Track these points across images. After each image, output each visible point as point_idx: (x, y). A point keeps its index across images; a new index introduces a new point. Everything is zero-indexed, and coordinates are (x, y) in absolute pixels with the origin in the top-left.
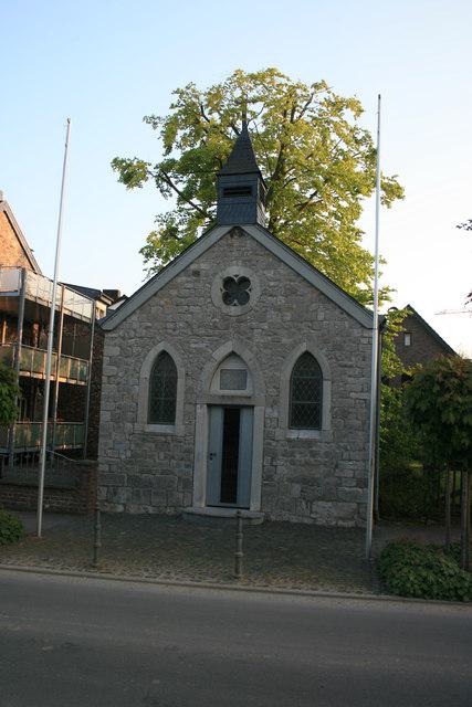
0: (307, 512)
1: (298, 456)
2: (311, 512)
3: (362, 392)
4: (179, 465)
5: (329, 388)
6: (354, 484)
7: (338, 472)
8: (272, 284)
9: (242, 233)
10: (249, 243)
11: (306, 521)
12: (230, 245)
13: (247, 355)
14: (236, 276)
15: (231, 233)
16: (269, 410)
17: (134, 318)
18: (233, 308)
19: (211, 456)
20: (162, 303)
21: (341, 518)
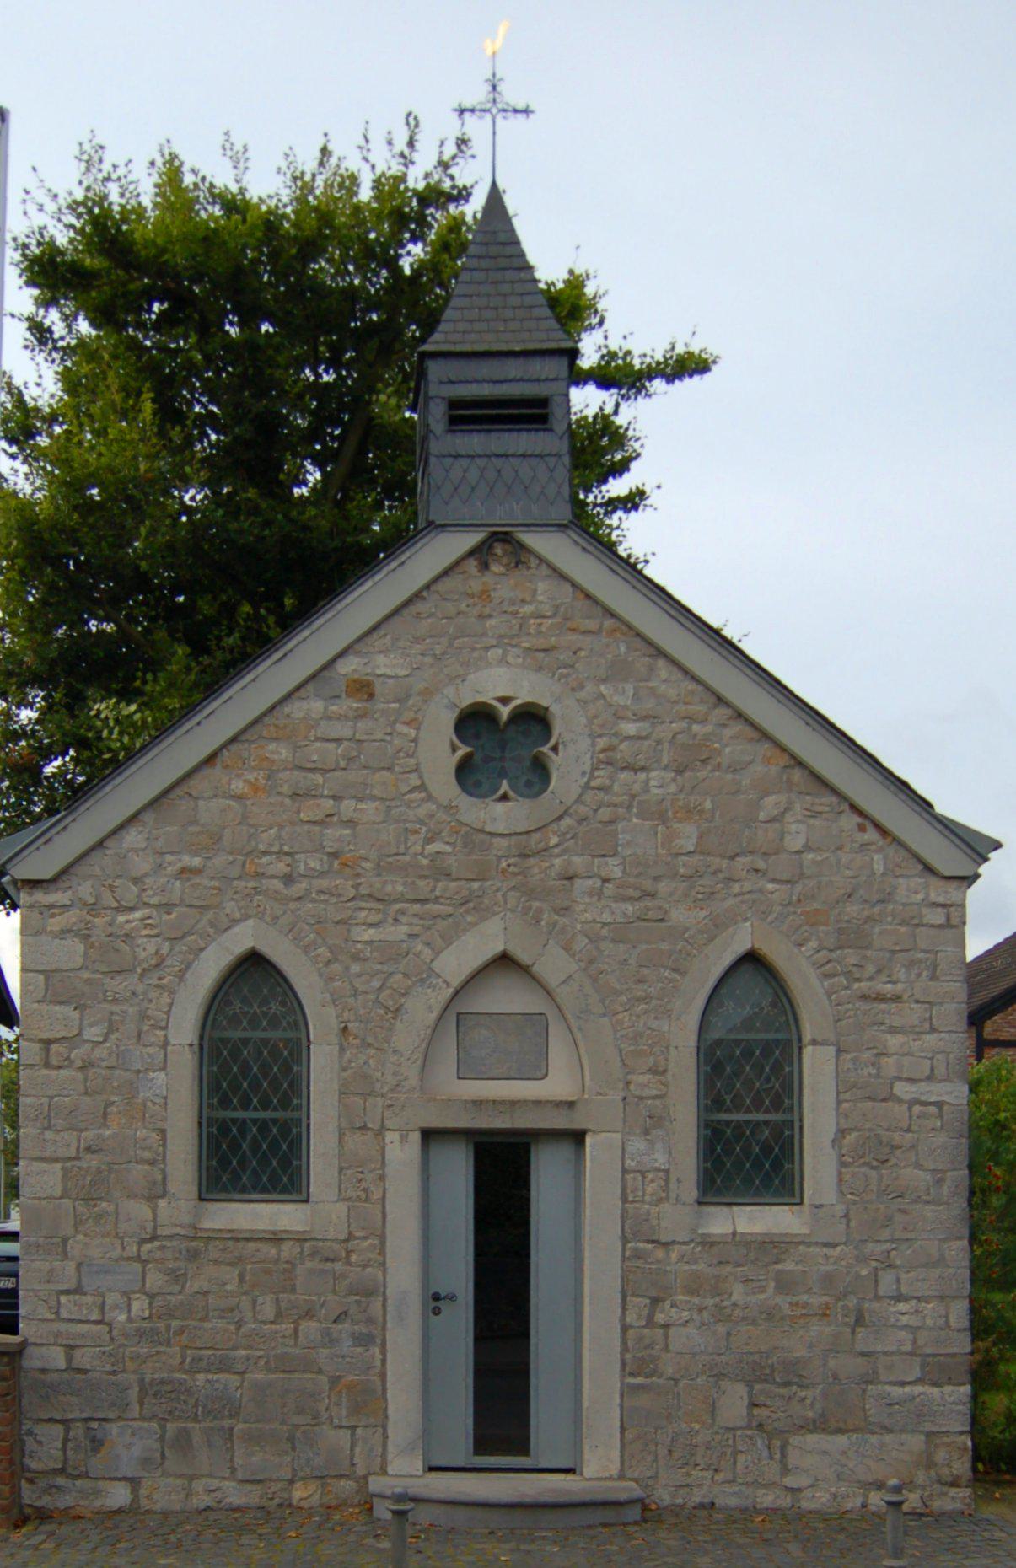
0: (771, 1470)
1: (738, 1293)
2: (785, 1470)
3: (930, 1078)
4: (330, 1341)
6: (916, 1372)
7: (864, 1339)
8: (630, 728)
9: (519, 554)
10: (544, 587)
11: (767, 1499)
12: (485, 595)
13: (553, 965)
14: (504, 700)
15: (481, 554)
16: (637, 1144)
18: (500, 808)
19: (435, 1301)
20: (238, 786)
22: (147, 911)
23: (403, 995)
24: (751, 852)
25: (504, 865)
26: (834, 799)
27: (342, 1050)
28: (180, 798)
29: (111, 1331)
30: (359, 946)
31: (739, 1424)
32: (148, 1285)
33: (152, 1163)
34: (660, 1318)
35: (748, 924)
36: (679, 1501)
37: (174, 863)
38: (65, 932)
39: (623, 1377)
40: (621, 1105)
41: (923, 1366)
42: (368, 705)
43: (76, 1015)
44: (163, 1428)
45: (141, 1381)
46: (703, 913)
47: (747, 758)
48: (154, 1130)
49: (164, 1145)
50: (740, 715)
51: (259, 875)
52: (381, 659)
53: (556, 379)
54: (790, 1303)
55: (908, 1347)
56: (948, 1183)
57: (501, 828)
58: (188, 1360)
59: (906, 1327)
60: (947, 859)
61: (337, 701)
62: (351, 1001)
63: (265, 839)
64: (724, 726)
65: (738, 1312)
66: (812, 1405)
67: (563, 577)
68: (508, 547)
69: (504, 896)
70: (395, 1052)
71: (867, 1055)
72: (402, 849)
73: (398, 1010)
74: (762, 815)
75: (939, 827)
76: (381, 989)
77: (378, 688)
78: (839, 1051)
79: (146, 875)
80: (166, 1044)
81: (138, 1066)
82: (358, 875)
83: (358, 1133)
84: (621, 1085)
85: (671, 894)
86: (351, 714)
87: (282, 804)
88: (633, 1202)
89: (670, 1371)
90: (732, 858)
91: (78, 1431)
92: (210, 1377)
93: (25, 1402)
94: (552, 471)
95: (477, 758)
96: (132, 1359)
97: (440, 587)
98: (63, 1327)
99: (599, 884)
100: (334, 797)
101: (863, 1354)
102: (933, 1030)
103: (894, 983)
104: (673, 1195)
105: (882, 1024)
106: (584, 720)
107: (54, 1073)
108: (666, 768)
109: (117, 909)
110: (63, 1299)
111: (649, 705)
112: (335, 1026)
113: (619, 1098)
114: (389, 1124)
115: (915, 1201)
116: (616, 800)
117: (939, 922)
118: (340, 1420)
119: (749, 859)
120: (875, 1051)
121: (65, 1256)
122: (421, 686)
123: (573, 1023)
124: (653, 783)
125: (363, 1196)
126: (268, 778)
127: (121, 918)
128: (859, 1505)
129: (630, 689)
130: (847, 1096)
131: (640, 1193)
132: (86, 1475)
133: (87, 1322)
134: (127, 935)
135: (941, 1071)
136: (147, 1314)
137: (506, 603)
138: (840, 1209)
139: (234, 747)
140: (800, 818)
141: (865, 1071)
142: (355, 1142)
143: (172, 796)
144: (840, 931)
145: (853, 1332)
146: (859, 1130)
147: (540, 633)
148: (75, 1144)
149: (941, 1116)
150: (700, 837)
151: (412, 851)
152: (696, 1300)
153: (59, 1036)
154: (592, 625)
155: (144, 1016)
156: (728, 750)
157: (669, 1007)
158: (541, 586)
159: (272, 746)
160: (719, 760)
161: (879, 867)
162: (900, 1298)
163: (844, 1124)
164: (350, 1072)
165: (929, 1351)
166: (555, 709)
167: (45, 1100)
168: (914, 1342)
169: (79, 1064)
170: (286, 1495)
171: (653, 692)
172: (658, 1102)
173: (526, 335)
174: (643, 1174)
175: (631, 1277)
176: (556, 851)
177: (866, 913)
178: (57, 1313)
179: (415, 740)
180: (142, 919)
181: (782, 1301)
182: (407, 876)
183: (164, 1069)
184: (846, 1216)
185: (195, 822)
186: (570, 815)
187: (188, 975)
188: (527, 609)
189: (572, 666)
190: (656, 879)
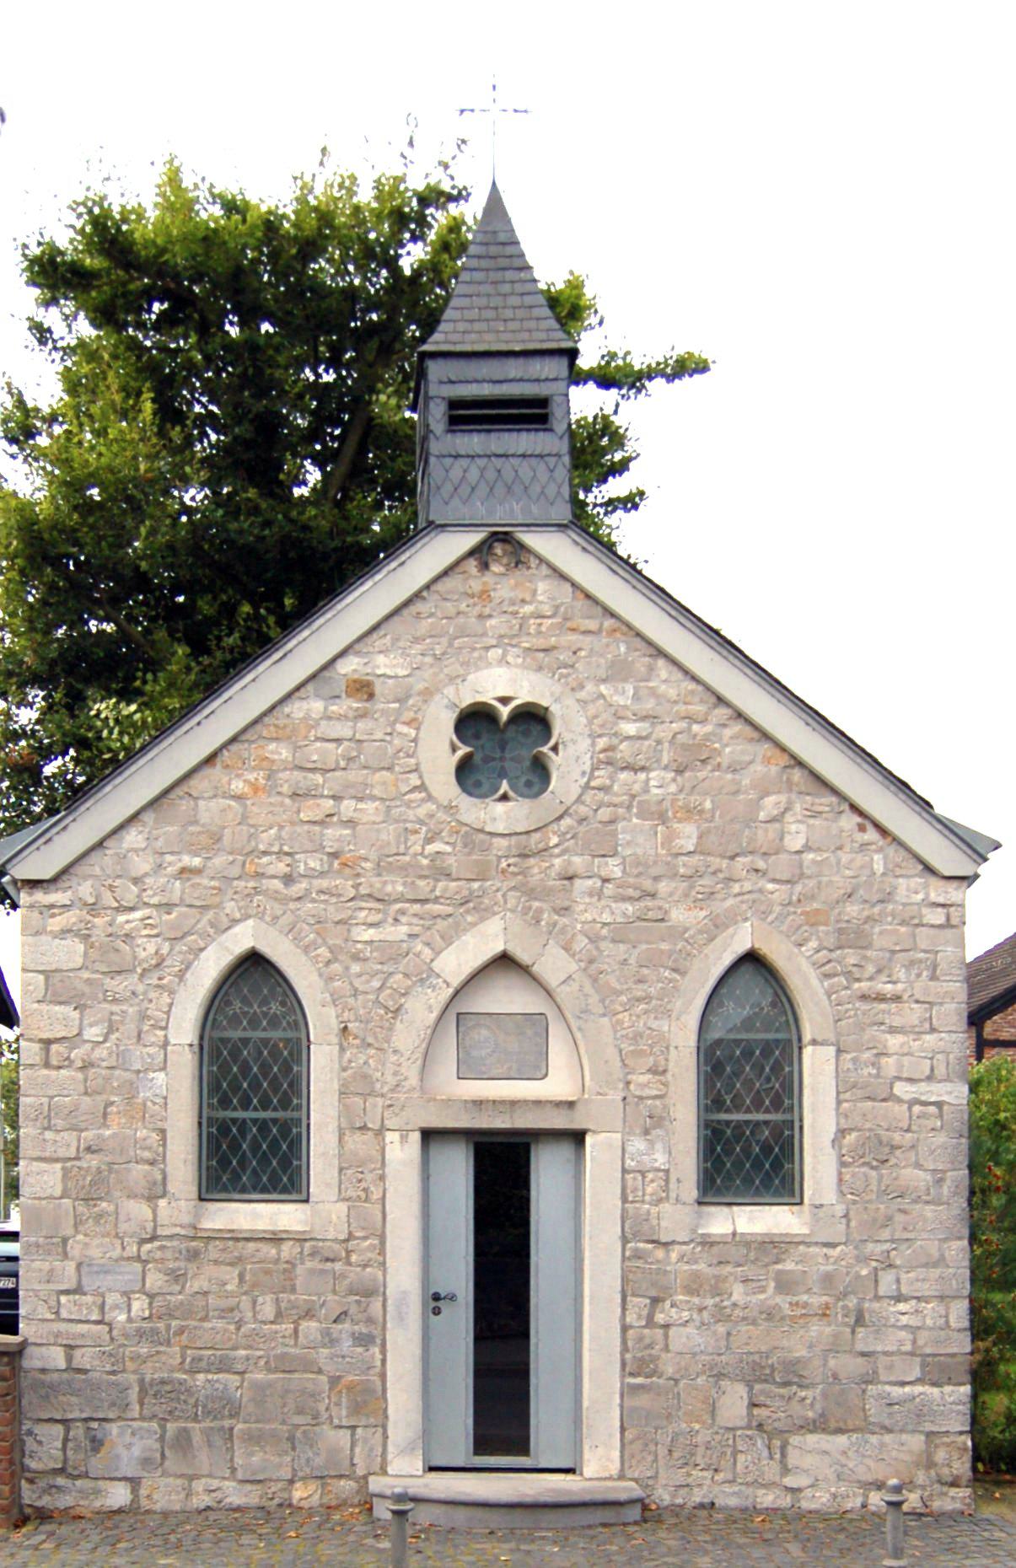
0: (771, 1470)
1: (738, 1293)
2: (785, 1470)
3: (930, 1078)
6: (916, 1373)
7: (864, 1339)
8: (630, 728)
9: (519, 554)
11: (767, 1499)
12: (484, 595)
13: (553, 965)
14: (504, 700)
15: (483, 555)
16: (637, 1144)
18: (501, 808)
19: (435, 1301)
20: (238, 786)
22: (146, 912)
25: (504, 864)
26: (834, 799)
27: (342, 1049)
28: (181, 798)
29: (110, 1331)
30: (359, 946)
32: (148, 1285)
34: (660, 1318)
35: (748, 924)
36: (679, 1501)
37: (174, 863)
38: (65, 932)
39: (623, 1377)
40: (621, 1105)
41: (923, 1365)
42: (367, 705)
43: (76, 1015)
45: (141, 1382)
46: (703, 913)
47: (747, 758)
48: (154, 1130)
49: (164, 1145)
50: (740, 715)
51: (259, 875)
52: (381, 659)
53: (556, 379)
54: (790, 1303)
55: (908, 1347)
56: (948, 1182)
57: (500, 828)
58: (188, 1360)
59: (905, 1327)
60: (948, 859)
61: (337, 701)
62: (351, 1001)
63: (266, 839)
64: (724, 726)
66: (812, 1405)
69: (504, 896)
70: (395, 1052)
72: (402, 849)
74: (762, 816)
75: (940, 827)
76: (381, 988)
78: (839, 1051)
79: (146, 875)
80: (166, 1044)
81: (137, 1066)
82: (358, 875)
83: (358, 1133)
84: (621, 1085)
85: (671, 894)
86: (351, 714)
87: (282, 804)
88: (632, 1202)
90: (732, 858)
91: (78, 1431)
92: (210, 1377)
93: (24, 1402)
94: (552, 471)
95: (477, 758)
96: (132, 1359)
97: (439, 587)
98: (63, 1327)
99: (599, 884)
100: (334, 797)
101: (863, 1354)
102: (933, 1030)
103: (894, 983)
104: (673, 1195)
105: (882, 1024)
106: (584, 720)
107: (54, 1073)
108: (666, 768)
110: (63, 1299)
111: (649, 705)
112: (335, 1025)
113: (619, 1098)
114: (388, 1124)
115: (915, 1201)
116: (616, 800)
117: (939, 922)
118: (340, 1420)
119: (749, 859)
120: (875, 1051)
122: (420, 686)
123: (574, 1023)
124: (652, 783)
126: (268, 778)
127: (121, 918)
128: (859, 1505)
129: (630, 689)
130: (847, 1096)
131: (640, 1193)
132: (86, 1475)
133: (87, 1322)
134: (127, 935)
135: (941, 1071)
136: (147, 1314)
137: (506, 603)
138: (840, 1210)
139: (234, 747)
140: (800, 818)
141: (865, 1072)
142: (358, 1143)
143: (172, 795)
144: (840, 931)
145: (853, 1332)
146: (859, 1130)
147: (540, 633)
148: (75, 1144)
149: (941, 1116)
150: (700, 837)
151: (411, 851)
153: (59, 1035)
154: (592, 625)
155: (143, 1017)
156: (728, 750)
157: (669, 1007)
158: (542, 586)
159: (272, 746)
160: (719, 760)
161: (879, 867)
162: (899, 1298)
163: (844, 1124)
164: (350, 1072)
165: (928, 1351)
168: (914, 1342)
171: (653, 692)
172: (658, 1102)
174: (643, 1174)
175: (631, 1276)
176: (556, 851)
177: (866, 913)
178: (57, 1313)
179: (415, 740)
180: (142, 920)
181: (782, 1301)
183: (164, 1069)
184: (846, 1216)
185: (196, 822)
186: (570, 815)
187: (188, 975)
188: (528, 609)
189: (572, 666)
190: (656, 879)
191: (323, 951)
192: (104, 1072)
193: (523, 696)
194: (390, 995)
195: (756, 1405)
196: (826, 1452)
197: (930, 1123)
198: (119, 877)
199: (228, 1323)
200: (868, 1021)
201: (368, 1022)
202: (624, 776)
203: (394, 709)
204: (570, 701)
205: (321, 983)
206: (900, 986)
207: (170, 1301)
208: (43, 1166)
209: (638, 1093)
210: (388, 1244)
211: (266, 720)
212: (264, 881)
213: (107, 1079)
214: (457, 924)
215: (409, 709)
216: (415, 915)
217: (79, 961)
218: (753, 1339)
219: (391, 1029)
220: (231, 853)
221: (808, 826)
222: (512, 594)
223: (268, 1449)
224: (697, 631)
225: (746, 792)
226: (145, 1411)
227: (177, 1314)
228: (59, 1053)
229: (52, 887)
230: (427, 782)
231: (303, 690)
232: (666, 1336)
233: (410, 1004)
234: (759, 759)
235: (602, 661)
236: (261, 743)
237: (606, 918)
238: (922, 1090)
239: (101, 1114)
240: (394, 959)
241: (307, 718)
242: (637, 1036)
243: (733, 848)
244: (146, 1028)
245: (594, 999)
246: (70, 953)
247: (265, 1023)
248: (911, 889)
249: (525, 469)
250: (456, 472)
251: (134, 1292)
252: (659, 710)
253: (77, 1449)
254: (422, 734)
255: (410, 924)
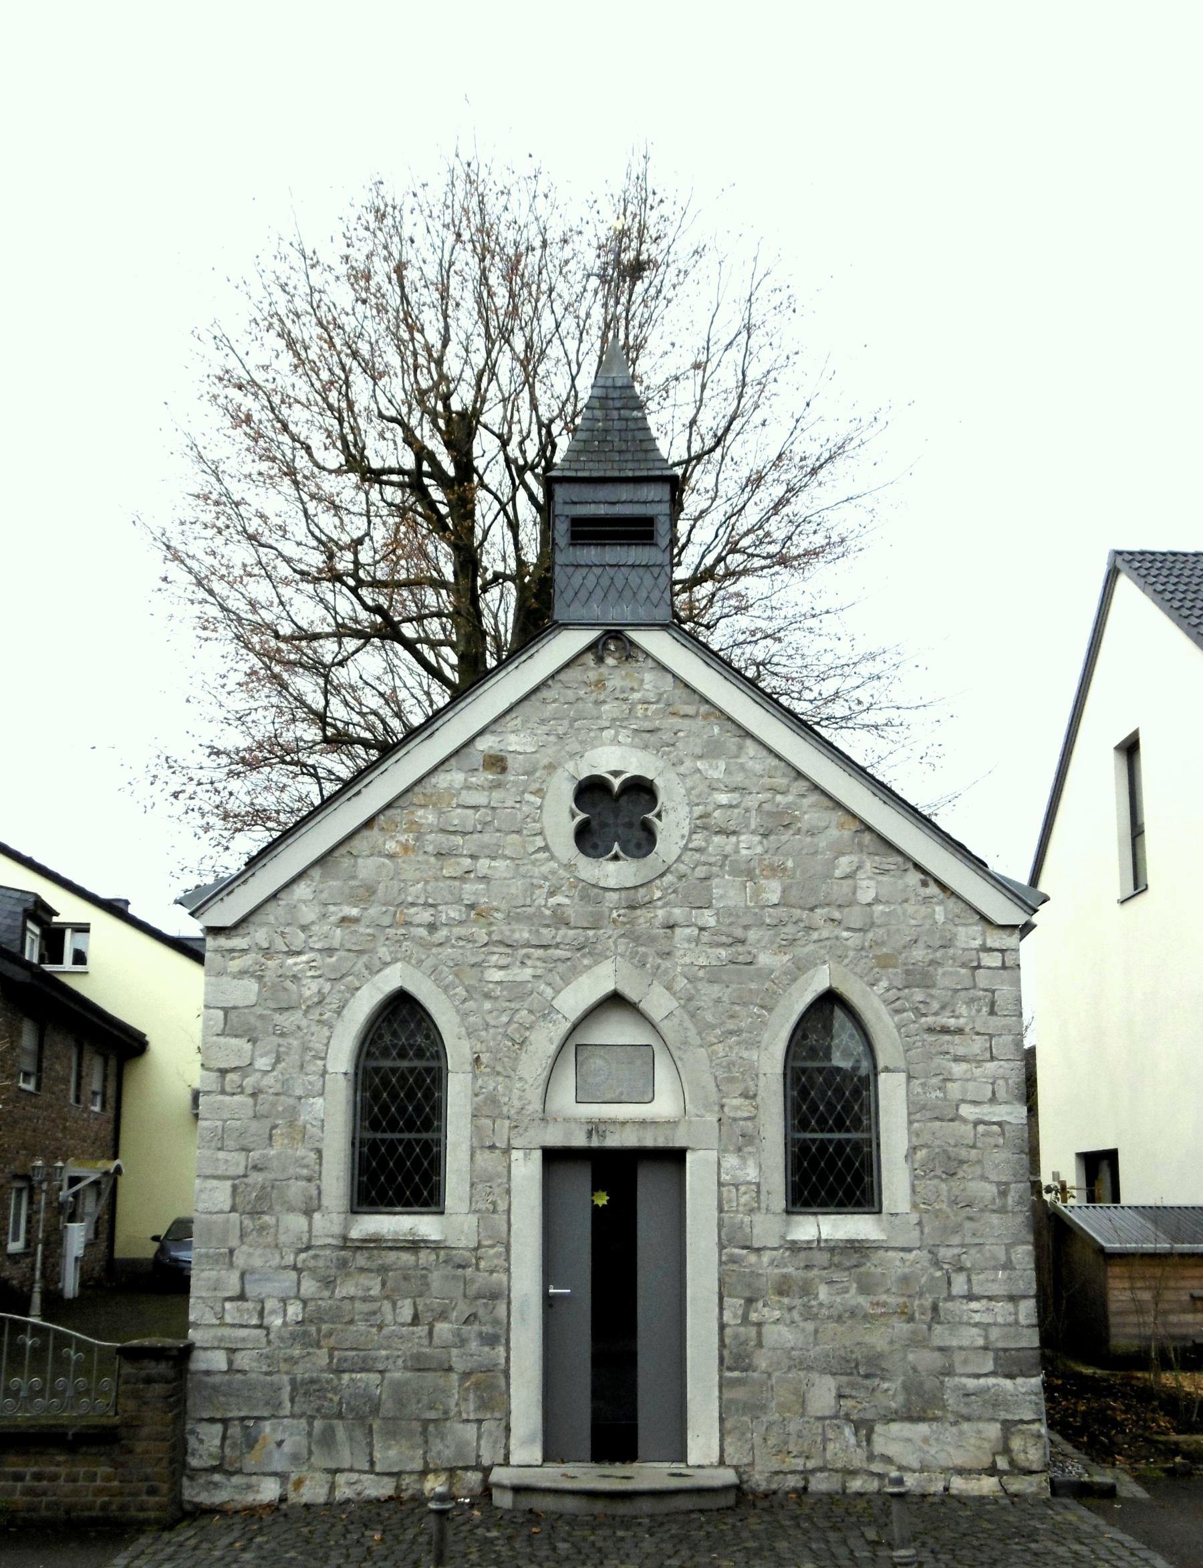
1: (823, 1292)
2: (871, 1458)
3: (993, 1100)
5: (902, 1092)
6: (989, 1366)
7: (941, 1335)
8: (723, 798)
9: (630, 651)
10: (650, 678)
12: (600, 684)
13: (657, 1003)
14: (616, 774)
16: (731, 1161)
17: (302, 890)
18: (612, 867)
20: (391, 846)
21: (961, 1471)
22: (311, 955)
23: (527, 1029)
24: (828, 905)
25: (615, 914)
26: (900, 859)
27: (475, 1077)
28: (343, 856)
29: (267, 1335)
30: (491, 986)
31: (827, 1413)
32: (302, 1290)
33: (309, 1180)
34: (754, 1317)
35: (826, 967)
36: (774, 1486)
37: (336, 912)
38: (243, 973)
39: (720, 1370)
40: (716, 1125)
41: (996, 1359)
42: (500, 777)
43: (249, 1046)
44: (310, 1424)
45: (293, 1382)
46: (787, 957)
47: (824, 824)
48: (312, 1150)
49: (320, 1164)
50: (816, 787)
51: (408, 924)
52: (512, 738)
53: (660, 502)
54: (872, 1303)
55: (980, 1342)
56: (1012, 1193)
57: (612, 883)
58: (335, 1361)
59: (976, 1325)
60: (1004, 911)
61: (476, 773)
62: (483, 1033)
63: (415, 891)
64: (803, 796)
65: (824, 1311)
66: (894, 1396)
67: (665, 669)
68: (619, 643)
69: (615, 942)
70: (520, 1079)
71: (935, 1081)
72: (528, 902)
73: (523, 1042)
74: (838, 873)
75: (993, 882)
77: (510, 761)
78: (910, 1078)
79: (313, 923)
80: (324, 1073)
81: (299, 1092)
82: (491, 924)
83: (487, 1151)
84: (717, 1108)
85: (759, 941)
86: (486, 784)
87: (427, 862)
88: (728, 1212)
89: (763, 1365)
90: (812, 909)
91: (235, 1430)
92: (354, 1375)
93: (189, 1403)
94: (656, 579)
95: (594, 823)
96: (285, 1360)
97: (562, 676)
98: (226, 1331)
99: (696, 932)
100: (472, 857)
101: (941, 1349)
102: (992, 1058)
103: (957, 1017)
104: (763, 1205)
105: (947, 1053)
106: (683, 791)
107: (227, 1098)
108: (753, 833)
109: (286, 953)
110: (228, 1305)
111: (738, 779)
112: (470, 1057)
113: (715, 1119)
114: (515, 1143)
115: (982, 1210)
116: (712, 860)
117: (994, 965)
118: (468, 1413)
119: (826, 910)
120: (941, 1077)
121: (231, 1265)
122: (545, 761)
123: (676, 1054)
124: (742, 845)
125: (491, 1207)
126: (417, 839)
127: (290, 961)
128: (941, 1489)
129: (722, 765)
130: (918, 1116)
131: (735, 1204)
132: (239, 1472)
134: (294, 976)
135: (1002, 1094)
136: (300, 1319)
137: (618, 691)
138: (914, 1218)
139: (389, 813)
140: (870, 874)
141: (933, 1095)
142: (485, 1160)
143: (337, 854)
144: (908, 973)
145: (930, 1328)
146: (929, 1147)
147: (646, 716)
148: (243, 1164)
149: (1003, 1133)
150: (783, 891)
151: (536, 903)
152: (786, 1300)
154: (690, 710)
155: (306, 1048)
156: (806, 817)
157: (758, 1039)
158: (648, 677)
159: (421, 812)
160: (799, 825)
161: (940, 916)
162: (971, 1297)
163: (915, 1142)
164: (481, 1097)
165: (1000, 1345)
166: (659, 783)
167: (219, 1123)
168: (986, 1338)
169: (249, 1090)
170: (418, 1486)
171: (742, 767)
172: (749, 1123)
173: (636, 465)
174: (736, 1186)
175: (727, 1279)
176: (659, 903)
177: (931, 957)
178: (222, 1318)
179: (540, 807)
180: (308, 962)
181: (862, 1301)
182: (533, 925)
183: (322, 1094)
184: (920, 1223)
185: (354, 877)
186: (671, 873)
187: (345, 1012)
188: (636, 696)
189: (673, 745)
190: (746, 927)
191: (460, 990)
192: (271, 1098)
193: (632, 771)
194: (517, 1030)
195: (844, 1397)
196: (909, 1440)
197: (992, 1141)
198: (289, 924)
199: (371, 1326)
200: (934, 1051)
201: (498, 1051)
202: (717, 839)
203: (523, 781)
204: (671, 775)
205: (457, 1019)
206: (962, 1021)
207: (320, 1307)
208: (215, 1183)
209: (732, 1115)
210: (512, 1252)
211: (416, 789)
212: (412, 929)
213: (274, 1105)
214: (574, 967)
215: (534, 781)
216: (539, 959)
217: (252, 999)
218: (838, 1338)
219: (516, 1059)
220: (384, 905)
221: (878, 882)
222: (623, 683)
223: (403, 1442)
224: (779, 715)
225: (823, 853)
226: (296, 1409)
227: (326, 1318)
228: (232, 1081)
229: (233, 933)
230: (550, 844)
231: (447, 764)
232: (759, 1334)
233: (533, 1036)
234: (834, 823)
235: (698, 741)
236: (412, 808)
237: (702, 961)
238: (985, 1111)
239: (267, 1136)
240: (522, 997)
241: (451, 787)
242: (729, 1067)
243: (812, 901)
244: (308, 1058)
245: (692, 1032)
246: (245, 992)
247: (411, 1053)
248: (970, 936)
249: (634, 577)
250: (577, 579)
251: (290, 1298)
252: (747, 783)
253: (234, 1446)
254: (546, 802)
255: (535, 967)
